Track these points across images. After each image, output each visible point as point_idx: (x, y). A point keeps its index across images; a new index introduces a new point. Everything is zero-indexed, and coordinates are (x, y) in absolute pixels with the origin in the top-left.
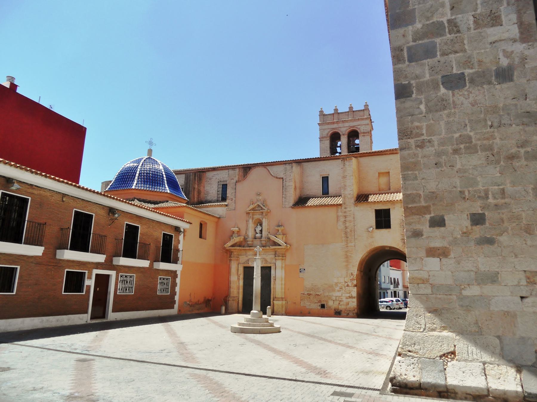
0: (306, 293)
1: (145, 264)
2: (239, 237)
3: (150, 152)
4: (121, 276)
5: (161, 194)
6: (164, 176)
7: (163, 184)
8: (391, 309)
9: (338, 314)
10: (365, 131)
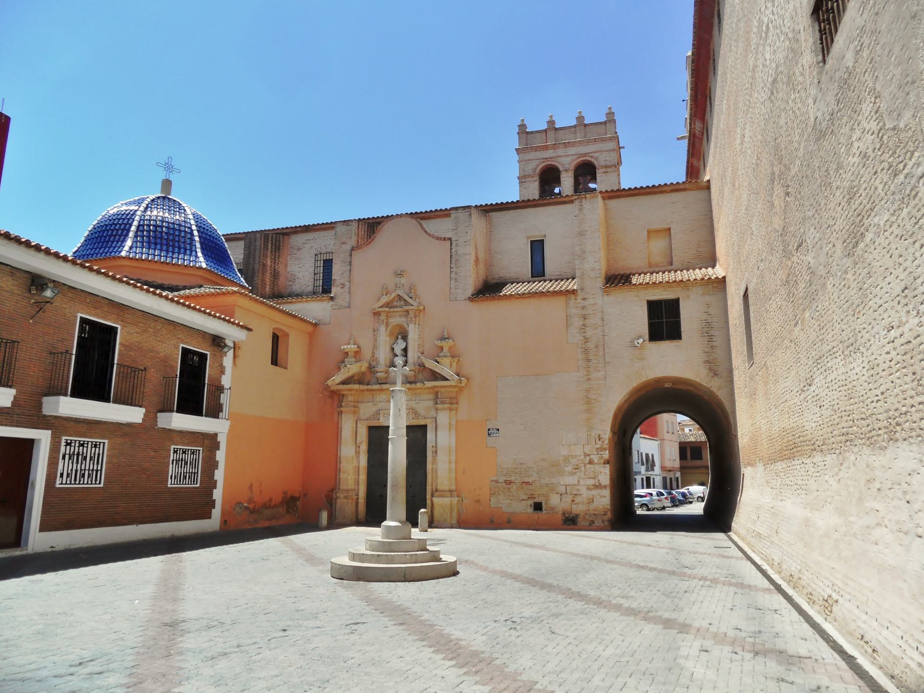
0: (502, 479)
1: (133, 415)
2: (359, 364)
3: (167, 184)
5: (186, 271)
6: (196, 233)
7: (192, 250)
8: (649, 510)
9: (570, 522)
10: (608, 163)
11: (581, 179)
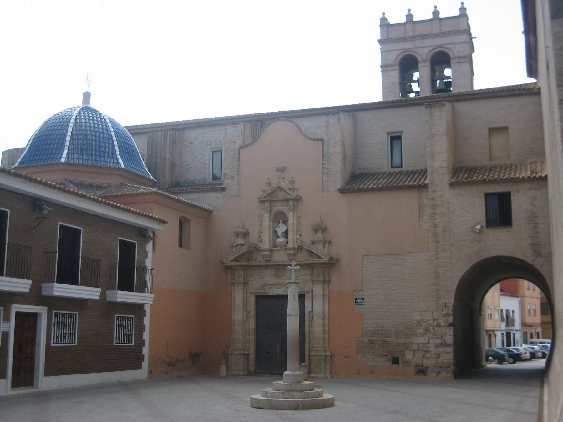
0: (366, 339)
1: (92, 293)
4: (56, 315)
11: (437, 68)
